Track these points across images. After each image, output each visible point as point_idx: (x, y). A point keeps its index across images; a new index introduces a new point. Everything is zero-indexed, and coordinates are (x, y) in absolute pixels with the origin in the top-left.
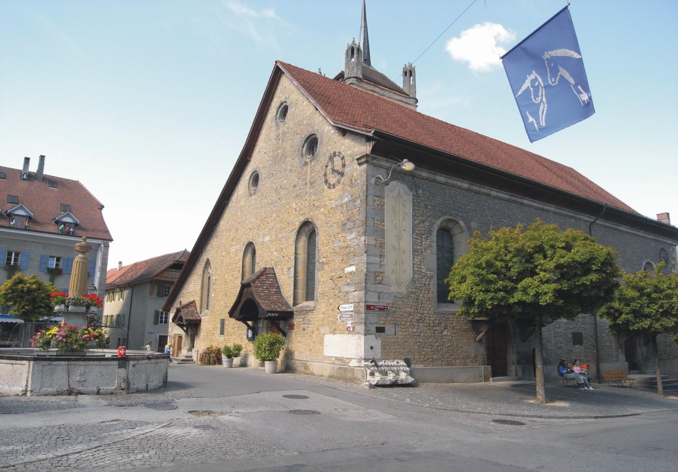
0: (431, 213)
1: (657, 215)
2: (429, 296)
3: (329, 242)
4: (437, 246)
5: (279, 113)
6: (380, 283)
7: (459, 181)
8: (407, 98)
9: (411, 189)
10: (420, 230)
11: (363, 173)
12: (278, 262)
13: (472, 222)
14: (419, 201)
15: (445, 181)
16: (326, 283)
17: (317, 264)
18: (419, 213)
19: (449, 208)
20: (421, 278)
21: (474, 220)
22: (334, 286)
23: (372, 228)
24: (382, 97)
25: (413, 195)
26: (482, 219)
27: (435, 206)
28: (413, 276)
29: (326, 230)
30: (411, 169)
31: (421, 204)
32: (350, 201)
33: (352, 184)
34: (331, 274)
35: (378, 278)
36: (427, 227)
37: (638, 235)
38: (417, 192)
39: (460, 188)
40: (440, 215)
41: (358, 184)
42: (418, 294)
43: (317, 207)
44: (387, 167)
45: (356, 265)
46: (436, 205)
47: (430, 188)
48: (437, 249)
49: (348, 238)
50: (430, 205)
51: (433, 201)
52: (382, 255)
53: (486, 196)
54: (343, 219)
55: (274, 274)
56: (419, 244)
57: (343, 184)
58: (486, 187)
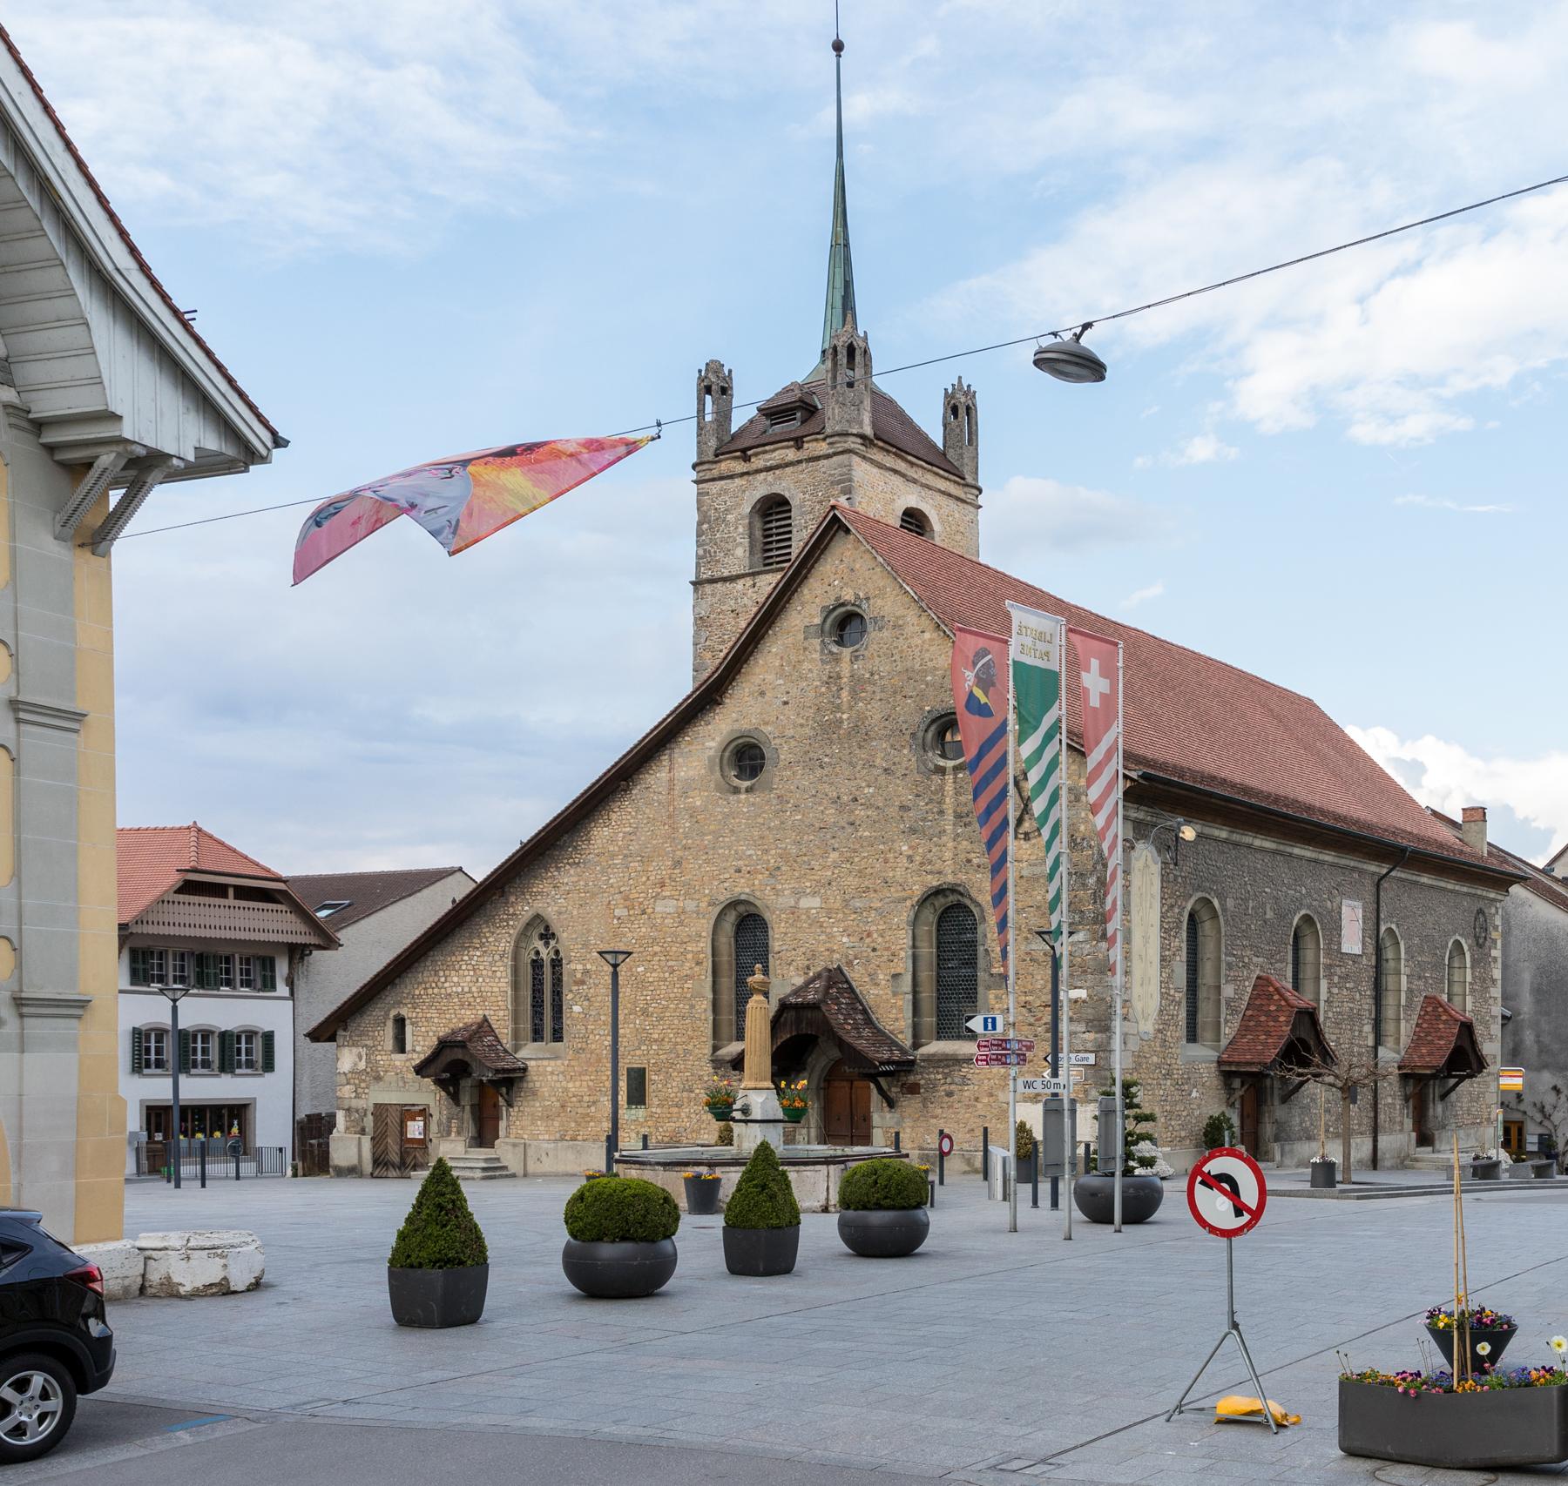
1: (1463, 809)
5: (829, 621)
8: (958, 484)
10: (1169, 922)
12: (856, 959)
27: (1185, 877)
33: (1076, 844)
37: (1444, 889)
39: (1216, 840)
55: (847, 982)
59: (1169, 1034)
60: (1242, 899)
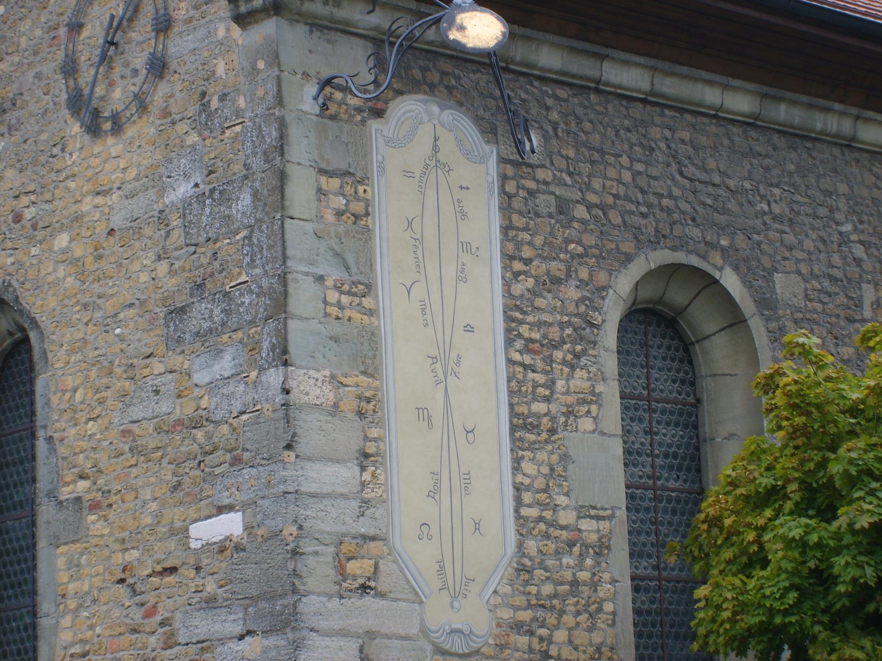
0: (590, 240)
2: (597, 638)
3: (101, 402)
4: (623, 397)
6: (364, 588)
7: (710, 83)
9: (490, 132)
10: (541, 324)
11: (261, 65)
13: (777, 277)
14: (531, 184)
15: (645, 85)
16: (94, 601)
17: (46, 512)
18: (530, 244)
19: (669, 211)
20: (558, 553)
21: (790, 265)
22: (137, 615)
23: (314, 325)
24: (776, 580)
25: (502, 160)
26: (822, 256)
27: (603, 207)
28: (520, 546)
29: (85, 341)
30: (492, 43)
31: (542, 198)
32: (200, 198)
34: (119, 559)
35: (352, 567)
36: (572, 308)
38: (519, 144)
39: (716, 115)
40: (628, 247)
41: (238, 113)
42: (543, 632)
43: (34, 227)
44: (376, 28)
45: (244, 507)
46: (610, 200)
47: (579, 121)
48: (625, 408)
49: (201, 377)
50: (583, 201)
51: (597, 184)
52: (366, 456)
53: (836, 151)
54: (171, 283)
56: (541, 390)
57: (166, 113)
58: (837, 106)
59: (561, 636)
60: (833, 279)
